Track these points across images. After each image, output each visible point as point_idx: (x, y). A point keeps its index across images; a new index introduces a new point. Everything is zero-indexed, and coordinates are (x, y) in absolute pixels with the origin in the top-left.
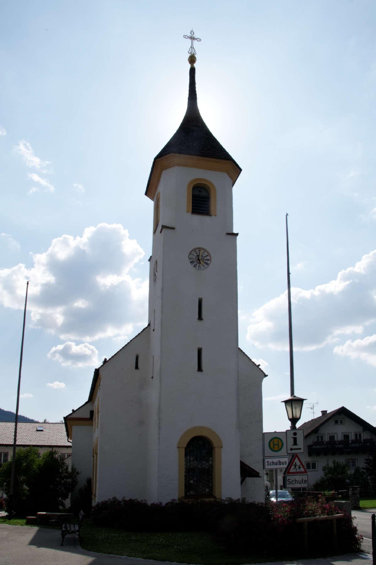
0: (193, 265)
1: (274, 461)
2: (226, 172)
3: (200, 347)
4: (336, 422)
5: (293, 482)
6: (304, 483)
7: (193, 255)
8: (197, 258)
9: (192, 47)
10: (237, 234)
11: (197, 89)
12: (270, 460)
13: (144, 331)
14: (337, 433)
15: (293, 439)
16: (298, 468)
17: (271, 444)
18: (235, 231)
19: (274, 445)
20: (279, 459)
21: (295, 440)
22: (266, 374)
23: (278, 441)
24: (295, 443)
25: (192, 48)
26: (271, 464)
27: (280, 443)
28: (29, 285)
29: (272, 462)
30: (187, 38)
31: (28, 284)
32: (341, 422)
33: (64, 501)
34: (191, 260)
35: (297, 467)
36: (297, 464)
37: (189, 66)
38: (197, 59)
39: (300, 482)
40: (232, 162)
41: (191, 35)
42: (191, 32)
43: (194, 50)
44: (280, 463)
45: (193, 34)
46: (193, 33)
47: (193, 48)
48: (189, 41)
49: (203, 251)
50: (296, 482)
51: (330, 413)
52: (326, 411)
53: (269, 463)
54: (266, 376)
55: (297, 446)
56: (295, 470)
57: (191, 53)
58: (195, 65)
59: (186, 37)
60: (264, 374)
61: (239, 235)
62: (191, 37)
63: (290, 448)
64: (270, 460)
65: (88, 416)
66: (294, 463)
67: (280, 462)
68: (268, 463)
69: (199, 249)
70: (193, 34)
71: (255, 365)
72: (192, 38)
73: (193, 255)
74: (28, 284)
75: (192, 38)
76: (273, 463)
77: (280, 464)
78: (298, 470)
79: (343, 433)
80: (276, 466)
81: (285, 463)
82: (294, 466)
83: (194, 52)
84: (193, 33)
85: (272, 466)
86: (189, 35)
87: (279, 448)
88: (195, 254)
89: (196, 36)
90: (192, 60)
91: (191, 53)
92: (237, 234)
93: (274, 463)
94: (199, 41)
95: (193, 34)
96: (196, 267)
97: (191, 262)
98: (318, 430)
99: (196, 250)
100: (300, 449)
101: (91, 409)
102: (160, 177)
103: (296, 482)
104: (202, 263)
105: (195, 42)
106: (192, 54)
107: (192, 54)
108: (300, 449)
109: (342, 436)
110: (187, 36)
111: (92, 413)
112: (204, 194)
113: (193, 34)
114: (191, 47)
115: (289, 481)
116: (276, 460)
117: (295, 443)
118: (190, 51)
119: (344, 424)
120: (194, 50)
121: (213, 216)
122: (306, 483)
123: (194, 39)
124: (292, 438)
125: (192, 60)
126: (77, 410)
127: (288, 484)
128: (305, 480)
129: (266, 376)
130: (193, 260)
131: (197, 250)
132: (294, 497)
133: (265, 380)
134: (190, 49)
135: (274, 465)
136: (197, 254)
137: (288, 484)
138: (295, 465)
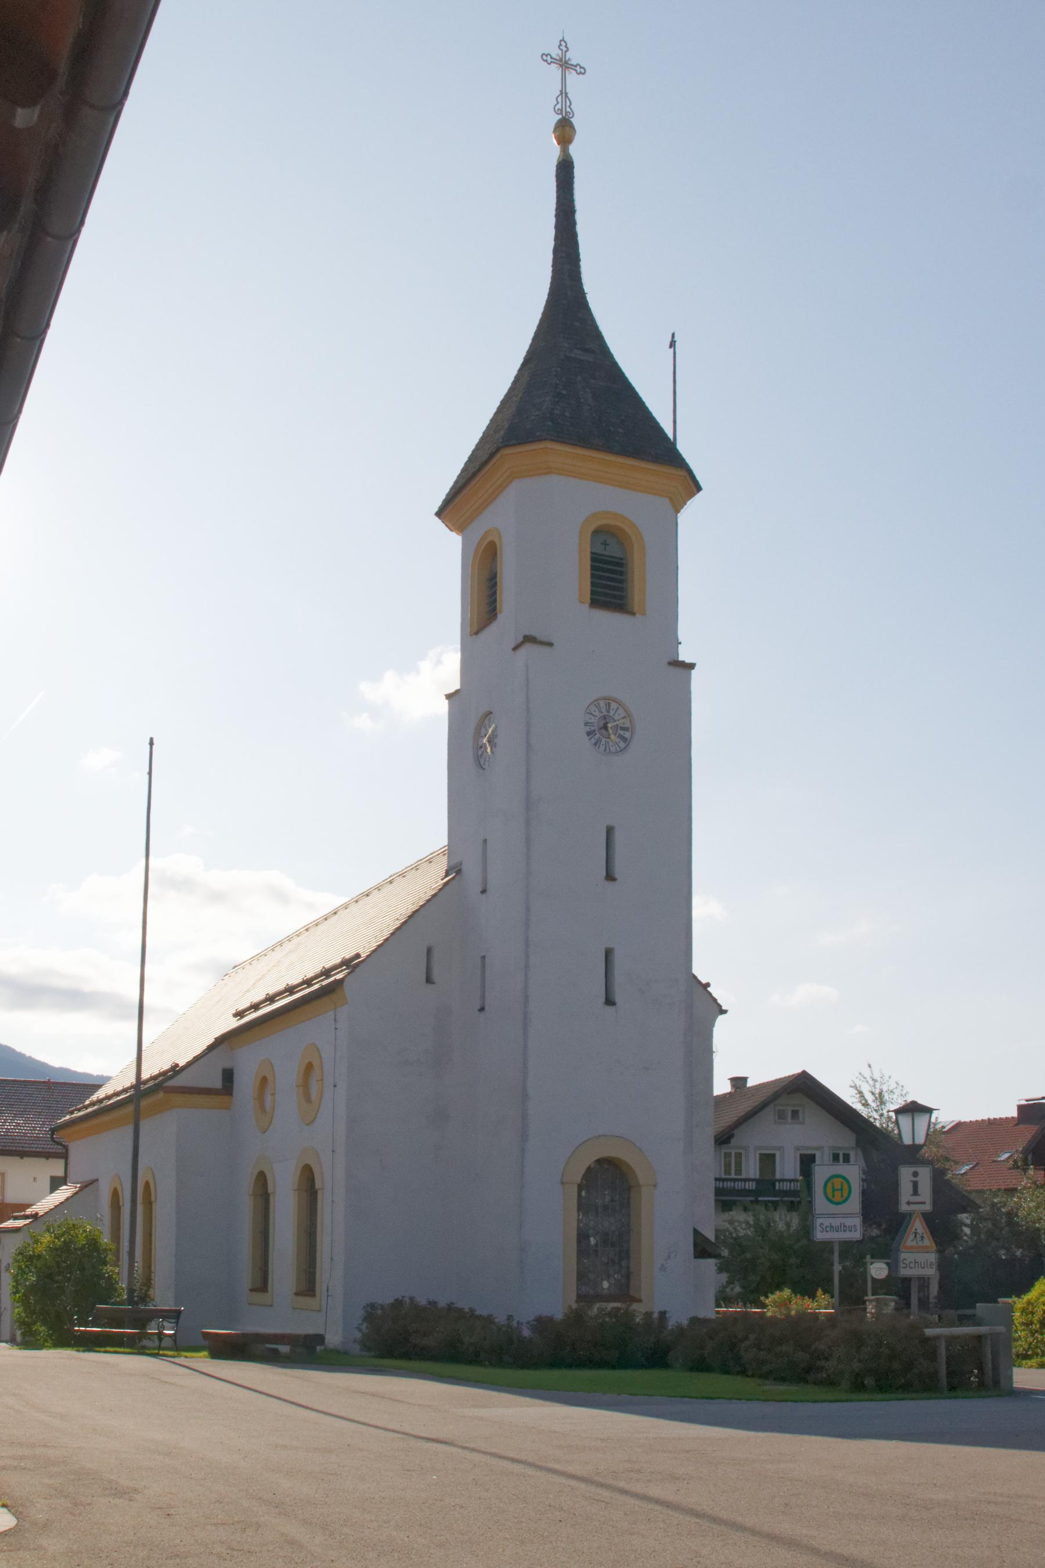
0: (593, 741)
1: (847, 1224)
2: (671, 499)
3: (611, 946)
4: (781, 1116)
5: (912, 1265)
6: (929, 1267)
7: (594, 716)
8: (603, 722)
9: (564, 94)
10: (692, 666)
11: (580, 229)
12: (827, 1222)
13: (447, 888)
14: (780, 1148)
15: (911, 1184)
16: (920, 1239)
17: (847, 1192)
18: (684, 656)
19: (834, 1190)
20: (843, 1220)
21: (915, 1185)
22: (724, 1008)
23: (842, 1183)
24: (915, 1192)
25: (564, 95)
26: (828, 1229)
27: (846, 1186)
28: (154, 747)
29: (829, 1225)
30: (551, 62)
31: (151, 743)
32: (795, 1114)
33: (868, 1257)
34: (588, 729)
35: (918, 1236)
36: (918, 1231)
37: (555, 151)
38: (577, 133)
39: (923, 1266)
40: (683, 473)
41: (560, 52)
42: (560, 45)
43: (568, 104)
44: (844, 1228)
45: (564, 49)
46: (566, 47)
47: (566, 94)
48: (555, 71)
49: (623, 714)
50: (917, 1265)
51: (752, 1087)
52: (744, 1080)
53: (824, 1227)
54: (724, 1012)
55: (918, 1197)
56: (914, 1243)
57: (562, 110)
58: (574, 150)
59: (549, 60)
60: (720, 1006)
61: (696, 668)
62: (561, 60)
63: (907, 1201)
64: (827, 1222)
65: (217, 1083)
66: (913, 1230)
67: (844, 1226)
68: (821, 1227)
69: (606, 701)
70: (566, 51)
71: (699, 982)
72: (564, 65)
73: (594, 716)
74: (151, 743)
75: (564, 65)
76: (832, 1227)
77: (844, 1231)
78: (920, 1243)
79: (797, 1148)
80: (837, 1233)
81: (853, 1228)
82: (914, 1234)
83: (568, 110)
84: (566, 47)
85: (829, 1233)
86: (555, 53)
87: (842, 1196)
88: (597, 713)
89: (573, 57)
90: (565, 131)
91: (562, 114)
92: (692, 666)
93: (833, 1227)
94: (581, 73)
95: (566, 51)
96: (590, 739)
97: (588, 734)
98: (732, 1136)
99: (598, 703)
100: (924, 1203)
101: (228, 1065)
102: (502, 488)
103: (917, 1265)
104: (612, 737)
105: (572, 76)
106: (564, 115)
107: (564, 115)
108: (924, 1203)
109: (795, 1157)
110: (551, 58)
111: (228, 1076)
112: (613, 551)
113: (561, 47)
114: (561, 91)
115: (905, 1261)
116: (836, 1222)
117: (915, 1192)
118: (559, 106)
119: (803, 1123)
120: (568, 104)
121: (638, 615)
122: (933, 1268)
123: (568, 68)
124: (911, 1181)
125: (565, 131)
126: (189, 1064)
127: (903, 1267)
128: (931, 1262)
129: (724, 1012)
130: (592, 728)
131: (602, 704)
132: (672, 1329)
133: (721, 1019)
134: (559, 99)
135: (833, 1231)
136: (601, 712)
137: (903, 1267)
138: (916, 1233)
